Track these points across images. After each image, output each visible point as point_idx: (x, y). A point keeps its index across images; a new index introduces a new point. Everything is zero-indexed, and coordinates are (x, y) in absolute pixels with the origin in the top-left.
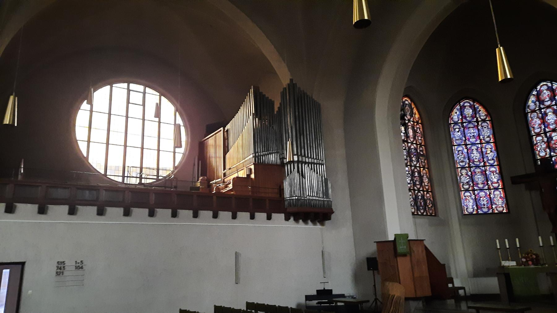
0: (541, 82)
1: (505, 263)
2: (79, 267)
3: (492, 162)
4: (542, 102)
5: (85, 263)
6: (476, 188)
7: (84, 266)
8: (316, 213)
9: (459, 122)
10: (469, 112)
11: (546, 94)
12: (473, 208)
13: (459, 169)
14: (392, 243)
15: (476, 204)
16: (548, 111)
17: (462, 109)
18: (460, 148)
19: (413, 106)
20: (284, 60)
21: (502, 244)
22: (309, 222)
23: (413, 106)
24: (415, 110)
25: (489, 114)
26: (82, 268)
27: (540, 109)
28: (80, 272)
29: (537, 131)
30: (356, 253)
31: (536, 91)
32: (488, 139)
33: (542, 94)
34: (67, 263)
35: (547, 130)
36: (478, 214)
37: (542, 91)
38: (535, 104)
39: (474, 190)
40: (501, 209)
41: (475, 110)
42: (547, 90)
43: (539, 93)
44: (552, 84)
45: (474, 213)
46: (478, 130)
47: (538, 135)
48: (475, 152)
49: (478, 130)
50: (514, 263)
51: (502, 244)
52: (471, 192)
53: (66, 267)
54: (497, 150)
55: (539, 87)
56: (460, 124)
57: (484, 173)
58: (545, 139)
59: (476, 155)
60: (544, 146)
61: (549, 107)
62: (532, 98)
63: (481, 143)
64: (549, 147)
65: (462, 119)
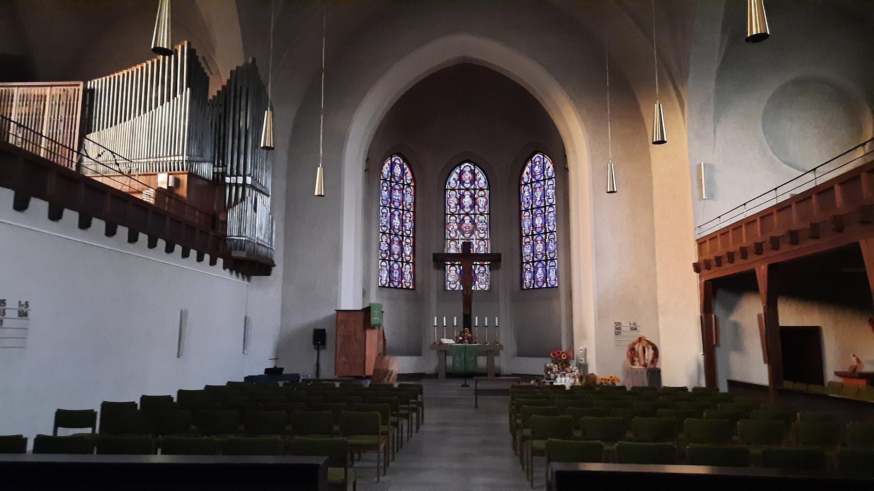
1: (445, 341)
2: (23, 314)
3: (408, 232)
4: (462, 182)
5: (638, 324)
7: (29, 313)
8: (252, 264)
10: (398, 171)
11: (467, 176)
14: (362, 315)
16: (466, 193)
17: (392, 166)
18: (385, 211)
19: (405, 166)
21: (440, 321)
22: (240, 275)
23: (405, 166)
24: (408, 170)
25: (414, 179)
26: (25, 315)
28: (22, 322)
29: (453, 210)
30: (282, 322)
32: (409, 207)
34: (623, 324)
39: (390, 261)
40: (408, 285)
41: (403, 170)
43: (462, 172)
46: (403, 194)
47: (453, 214)
48: (396, 218)
49: (403, 194)
50: (451, 341)
51: (440, 321)
53: (6, 311)
54: (414, 221)
55: (462, 166)
57: (400, 243)
58: (458, 221)
59: (396, 222)
60: (456, 227)
61: (467, 189)
62: (454, 176)
63: (403, 210)
64: (459, 228)
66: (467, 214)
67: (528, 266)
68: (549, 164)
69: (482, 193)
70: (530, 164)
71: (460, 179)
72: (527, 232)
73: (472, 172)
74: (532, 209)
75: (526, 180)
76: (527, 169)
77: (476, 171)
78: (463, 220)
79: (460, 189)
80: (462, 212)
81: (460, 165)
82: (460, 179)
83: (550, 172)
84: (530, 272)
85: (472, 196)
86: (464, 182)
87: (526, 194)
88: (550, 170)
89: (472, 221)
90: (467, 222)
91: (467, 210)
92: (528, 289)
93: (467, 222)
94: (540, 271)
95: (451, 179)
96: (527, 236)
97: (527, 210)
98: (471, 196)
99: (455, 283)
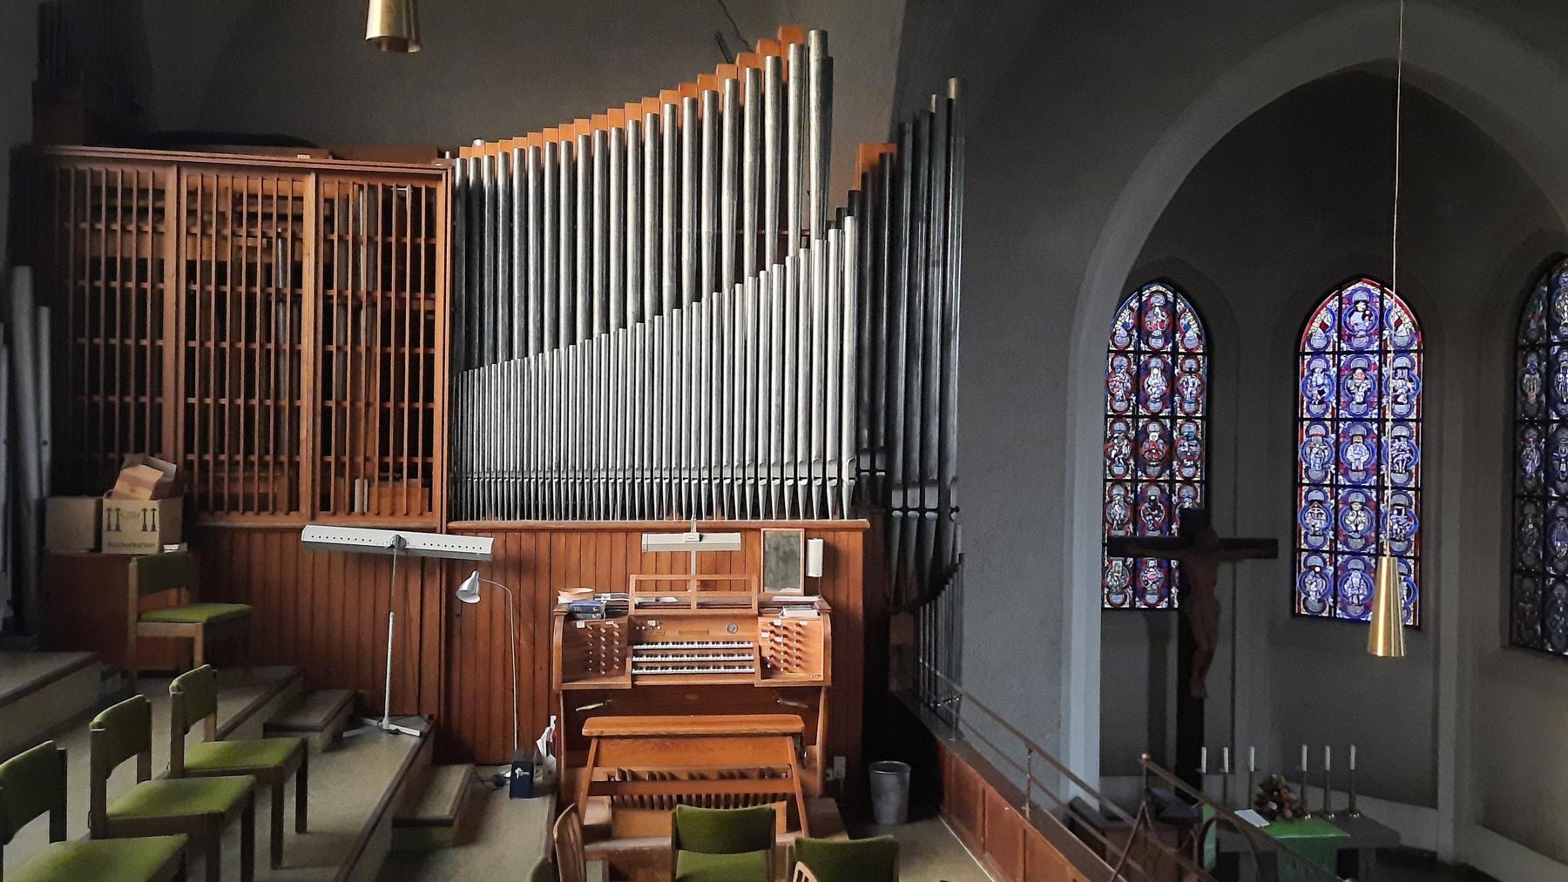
0: (1152, 282)
6: (1343, 413)
9: (1326, 548)
12: (1324, 467)
13: (1308, 358)
15: (1337, 458)
20: (1180, 845)
27: (1138, 352)
31: (1140, 300)
33: (1150, 314)
35: (1142, 411)
36: (1332, 618)
37: (1152, 308)
38: (1130, 336)
42: (1162, 308)
43: (1142, 312)
44: (1175, 297)
45: (1325, 614)
50: (175, 547)
52: (1326, 556)
56: (1328, 423)
65: (1335, 541)
66: (1154, 417)
67: (1315, 561)
68: (1397, 310)
69: (1190, 363)
70: (1334, 304)
71: (1139, 325)
72: (1316, 474)
73: (1169, 308)
74: (1336, 420)
75: (1318, 342)
76: (1324, 316)
77: (1180, 306)
78: (1145, 433)
79: (1341, 353)
80: (1142, 411)
81: (1341, 287)
82: (1139, 325)
83: (1404, 333)
84: (1322, 575)
85: (1168, 372)
86: (1149, 334)
87: (1319, 378)
88: (1193, 333)
89: (1166, 436)
90: (1154, 436)
91: (1154, 407)
92: (1315, 617)
93: (1154, 436)
94: (1355, 578)
95: (1316, 324)
96: (1317, 485)
97: (1317, 420)
98: (1163, 371)
99: (1123, 591)
